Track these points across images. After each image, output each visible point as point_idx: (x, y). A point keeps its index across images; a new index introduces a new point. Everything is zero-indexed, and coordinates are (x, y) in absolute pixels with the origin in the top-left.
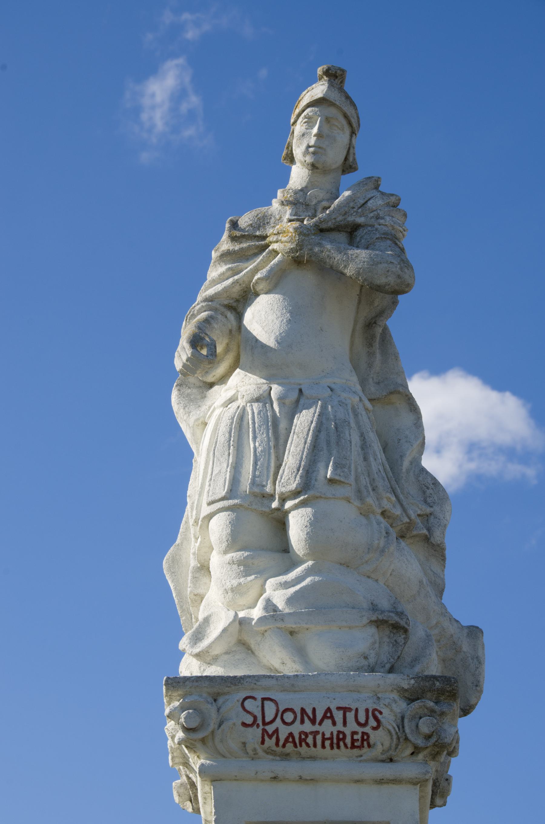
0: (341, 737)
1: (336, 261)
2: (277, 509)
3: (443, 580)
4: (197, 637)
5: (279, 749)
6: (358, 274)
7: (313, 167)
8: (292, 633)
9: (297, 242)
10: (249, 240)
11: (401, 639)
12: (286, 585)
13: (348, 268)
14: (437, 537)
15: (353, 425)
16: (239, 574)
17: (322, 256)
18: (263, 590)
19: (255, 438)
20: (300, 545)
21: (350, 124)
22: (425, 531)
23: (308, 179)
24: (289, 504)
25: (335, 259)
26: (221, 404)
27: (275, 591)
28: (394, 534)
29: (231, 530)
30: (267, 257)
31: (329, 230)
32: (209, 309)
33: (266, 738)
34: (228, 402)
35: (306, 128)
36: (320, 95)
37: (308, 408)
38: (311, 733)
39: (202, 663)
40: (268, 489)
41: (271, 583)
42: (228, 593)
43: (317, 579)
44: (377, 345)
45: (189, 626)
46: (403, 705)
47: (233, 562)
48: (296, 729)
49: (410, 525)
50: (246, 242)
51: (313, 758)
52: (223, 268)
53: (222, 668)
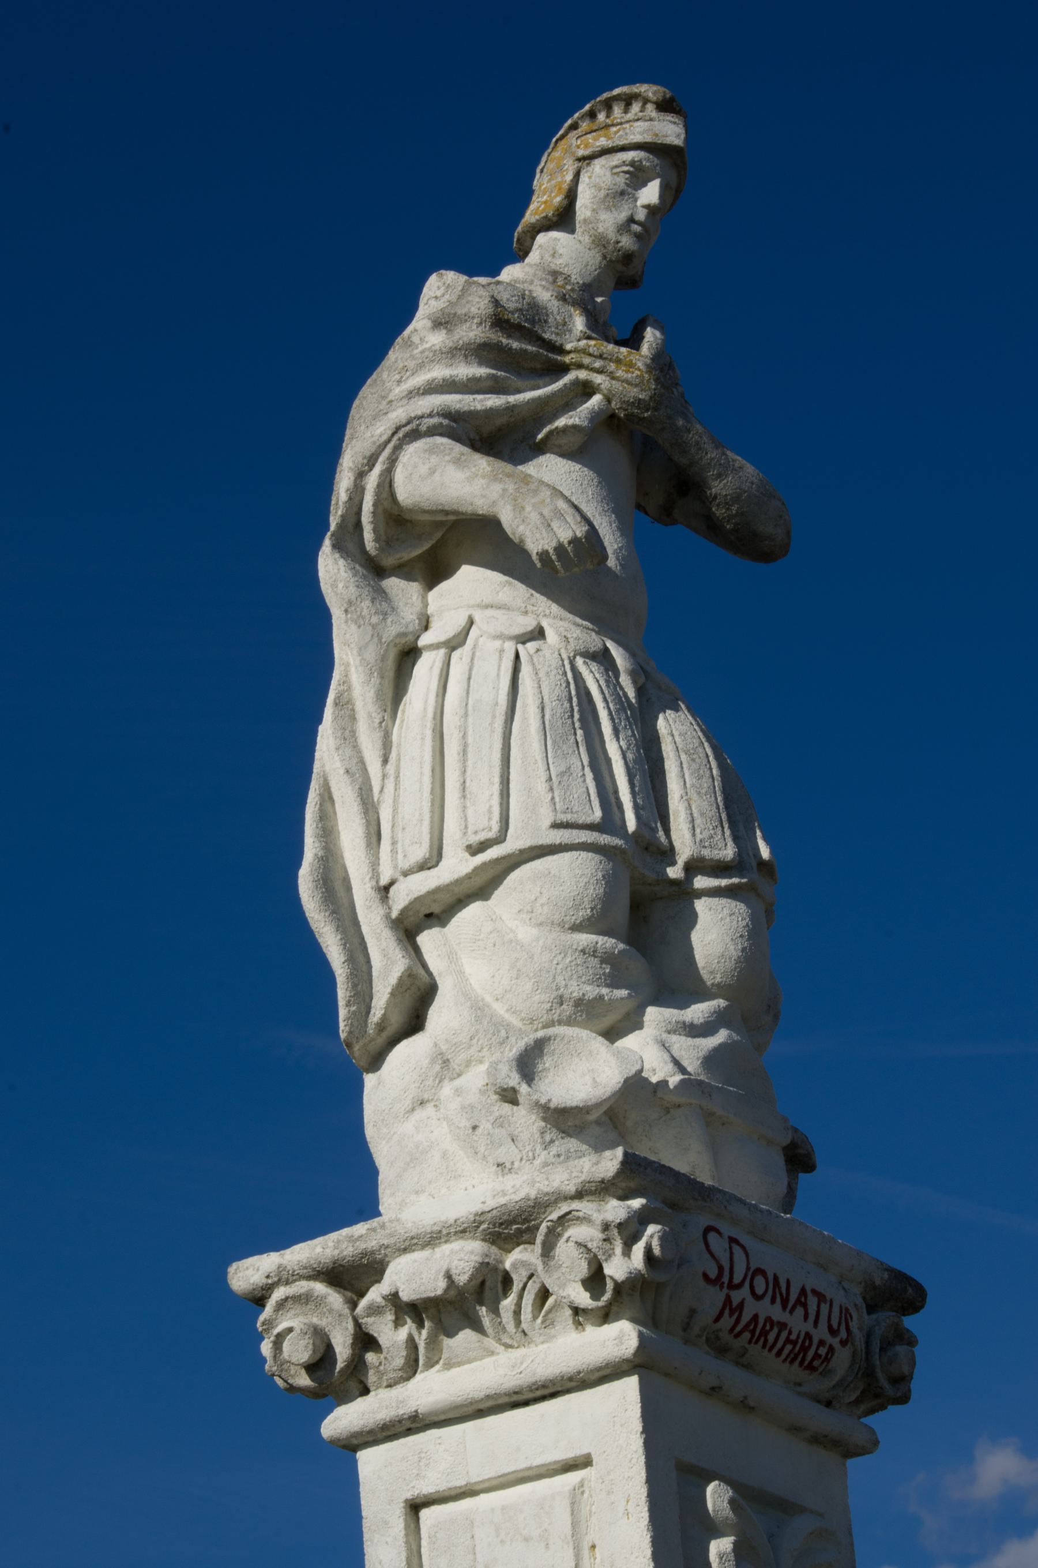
1: (707, 459)
2: (674, 883)
6: (736, 498)
9: (653, 392)
10: (525, 339)
13: (723, 480)
16: (600, 978)
17: (686, 439)
20: (723, 965)
23: (596, 272)
25: (707, 453)
26: (515, 634)
27: (669, 1033)
29: (605, 892)
30: (570, 389)
33: (727, 1312)
34: (528, 636)
35: (626, 183)
38: (779, 1323)
39: (549, 1126)
42: (561, 1004)
45: (359, 1027)
47: (595, 951)
50: (518, 340)
53: (591, 1149)
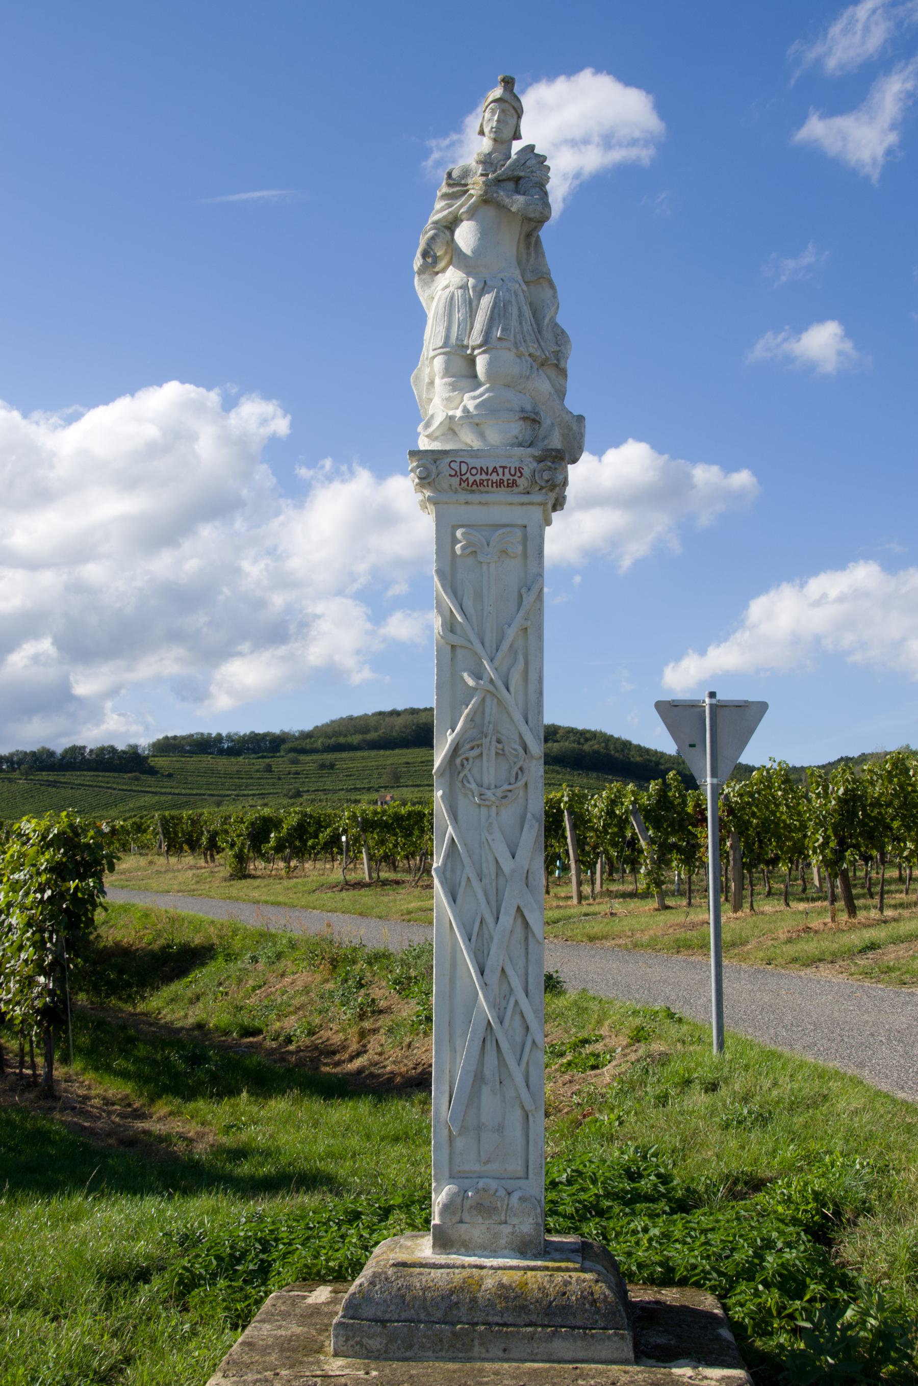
0: (501, 482)
2: (470, 354)
3: (565, 388)
4: (428, 425)
5: (469, 488)
6: (519, 211)
7: (495, 140)
8: (477, 425)
11: (537, 427)
12: (474, 398)
14: (562, 365)
15: (514, 303)
18: (462, 401)
19: (459, 311)
21: (517, 112)
22: (555, 362)
24: (476, 352)
28: (535, 366)
31: (504, 180)
32: (435, 228)
36: (498, 96)
37: (489, 293)
40: (465, 343)
41: (467, 396)
43: (491, 394)
44: (532, 248)
46: (535, 464)
48: (478, 478)
49: (546, 360)
51: (487, 492)
52: (443, 203)
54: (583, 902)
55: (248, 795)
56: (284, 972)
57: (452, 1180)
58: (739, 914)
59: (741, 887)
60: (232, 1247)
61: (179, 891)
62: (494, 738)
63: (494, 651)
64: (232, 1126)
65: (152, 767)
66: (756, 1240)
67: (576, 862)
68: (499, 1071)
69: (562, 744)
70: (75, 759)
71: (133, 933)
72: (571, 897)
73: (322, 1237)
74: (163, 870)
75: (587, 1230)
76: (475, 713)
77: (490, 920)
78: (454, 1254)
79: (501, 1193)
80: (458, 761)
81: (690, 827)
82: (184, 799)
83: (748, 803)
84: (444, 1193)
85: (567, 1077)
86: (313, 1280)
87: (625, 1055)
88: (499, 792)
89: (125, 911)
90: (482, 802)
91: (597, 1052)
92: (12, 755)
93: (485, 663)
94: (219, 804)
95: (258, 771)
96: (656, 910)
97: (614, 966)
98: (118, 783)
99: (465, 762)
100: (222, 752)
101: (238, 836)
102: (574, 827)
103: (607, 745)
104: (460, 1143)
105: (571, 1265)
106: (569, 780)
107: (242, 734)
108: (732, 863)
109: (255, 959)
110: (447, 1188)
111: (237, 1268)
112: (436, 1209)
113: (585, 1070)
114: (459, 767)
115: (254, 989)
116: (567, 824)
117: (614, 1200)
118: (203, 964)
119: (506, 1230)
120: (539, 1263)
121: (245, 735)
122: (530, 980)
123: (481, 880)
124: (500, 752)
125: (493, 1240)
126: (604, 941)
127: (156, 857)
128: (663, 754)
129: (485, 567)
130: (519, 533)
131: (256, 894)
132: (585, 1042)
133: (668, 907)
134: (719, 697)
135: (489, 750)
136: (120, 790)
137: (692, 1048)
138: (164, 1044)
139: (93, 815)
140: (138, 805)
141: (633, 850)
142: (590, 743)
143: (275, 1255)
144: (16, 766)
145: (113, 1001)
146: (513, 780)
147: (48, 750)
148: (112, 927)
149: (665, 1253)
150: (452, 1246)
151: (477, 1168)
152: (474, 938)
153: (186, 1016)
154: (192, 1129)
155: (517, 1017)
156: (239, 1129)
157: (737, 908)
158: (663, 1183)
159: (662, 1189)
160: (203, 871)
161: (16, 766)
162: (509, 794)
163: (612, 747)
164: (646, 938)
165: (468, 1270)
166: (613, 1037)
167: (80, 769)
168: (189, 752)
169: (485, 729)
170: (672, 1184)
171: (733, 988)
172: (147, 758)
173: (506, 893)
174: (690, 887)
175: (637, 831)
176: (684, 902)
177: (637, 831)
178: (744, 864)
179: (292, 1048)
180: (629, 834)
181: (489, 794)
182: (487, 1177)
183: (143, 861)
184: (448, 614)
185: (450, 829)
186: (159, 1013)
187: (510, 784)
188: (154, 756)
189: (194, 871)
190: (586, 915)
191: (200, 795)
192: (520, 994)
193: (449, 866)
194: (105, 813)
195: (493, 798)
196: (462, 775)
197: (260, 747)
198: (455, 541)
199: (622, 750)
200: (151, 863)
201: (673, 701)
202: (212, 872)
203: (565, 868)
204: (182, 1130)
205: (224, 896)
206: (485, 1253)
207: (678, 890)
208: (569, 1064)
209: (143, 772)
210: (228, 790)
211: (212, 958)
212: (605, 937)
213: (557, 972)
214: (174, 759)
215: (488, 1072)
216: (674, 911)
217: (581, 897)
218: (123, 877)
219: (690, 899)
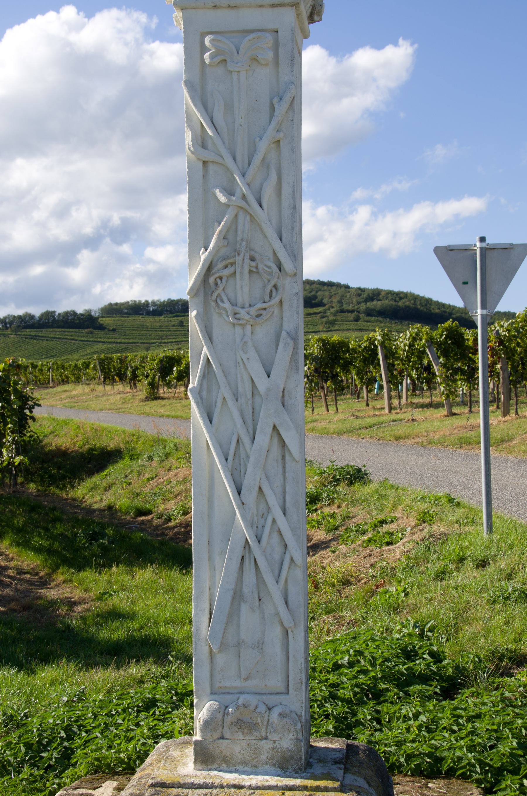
54: (393, 412)
55: (168, 343)
56: (170, 467)
57: (213, 696)
58: (507, 418)
59: (508, 398)
60: (40, 735)
61: (109, 410)
62: (248, 256)
63: (246, 166)
64: (105, 593)
65: (102, 325)
66: (520, 730)
67: (387, 383)
68: (258, 589)
69: (383, 302)
70: (48, 320)
71: (70, 440)
72: (384, 408)
73: (120, 725)
74: (101, 395)
75: (363, 716)
76: (228, 231)
77: (246, 439)
78: (216, 770)
79: (262, 709)
80: (211, 280)
81: (470, 355)
82: (124, 346)
83: (514, 336)
84: (205, 710)
85: (367, 552)
86: (104, 772)
87: (413, 534)
88: (253, 311)
89: (66, 424)
90: (236, 321)
91: (391, 531)
92: (5, 318)
93: (237, 177)
94: (148, 349)
95: (174, 326)
96: (446, 416)
97: (412, 459)
98: (78, 336)
99: (219, 281)
100: (149, 313)
101: (151, 370)
102: (386, 357)
103: (415, 302)
104: (220, 659)
105: (329, 784)
106: (388, 327)
107: (162, 300)
108: (501, 380)
109: (150, 458)
110: (207, 705)
111: (43, 755)
112: (198, 725)
113: (382, 546)
114: (213, 286)
115: (148, 480)
116: (380, 356)
117: (390, 682)
118: (115, 462)
119: (266, 745)
120: (298, 782)
121: (164, 301)
122: (288, 498)
123: (237, 401)
124: (255, 270)
125: (254, 756)
126: (406, 440)
127: (96, 386)
128: (454, 307)
129: (235, 76)
130: (269, 38)
131: (162, 411)
132: (383, 522)
133: (454, 414)
134: (488, 241)
135: (242, 267)
136: (80, 341)
137: (467, 529)
138: (77, 522)
139: (62, 358)
140: (92, 350)
141: (429, 373)
142: (403, 300)
143: (78, 742)
144: (8, 326)
145: (53, 489)
146: (267, 298)
147: (30, 315)
148: (56, 436)
149: (433, 742)
150: (213, 762)
151: (238, 684)
152: (230, 458)
153: (101, 500)
154: (77, 594)
155: (275, 535)
156: (111, 595)
157: (505, 413)
158: (435, 663)
159: (434, 668)
160: (128, 394)
161: (8, 326)
162: (263, 312)
163: (418, 303)
164: (437, 436)
165: (226, 790)
166: (405, 518)
167: (52, 327)
168: (126, 313)
169: (238, 246)
170: (443, 663)
171: (502, 475)
172: (97, 318)
173: (262, 413)
174: (470, 399)
175: (431, 359)
176: (467, 410)
177: (431, 359)
178: (511, 381)
179: (171, 524)
180: (425, 362)
181: (243, 312)
182: (248, 693)
183: (87, 389)
184: (199, 128)
185: (205, 349)
186: (84, 498)
187: (264, 302)
188: (103, 317)
189: (121, 395)
190: (394, 421)
191: (135, 343)
192: (277, 512)
193: (205, 385)
194: (70, 357)
195: (247, 317)
196: (215, 294)
197: (175, 309)
198: (204, 49)
199: (426, 305)
200: (93, 390)
201: (449, 246)
202: (134, 396)
203: (381, 387)
204: (69, 595)
205: (140, 412)
206: (246, 768)
207: (463, 401)
208: (369, 541)
209: (95, 328)
210: (154, 339)
211: (121, 458)
212: (407, 437)
213: (365, 466)
214: (117, 319)
215: (246, 590)
216: (458, 417)
217: (391, 408)
218: (73, 400)
219: (470, 408)
